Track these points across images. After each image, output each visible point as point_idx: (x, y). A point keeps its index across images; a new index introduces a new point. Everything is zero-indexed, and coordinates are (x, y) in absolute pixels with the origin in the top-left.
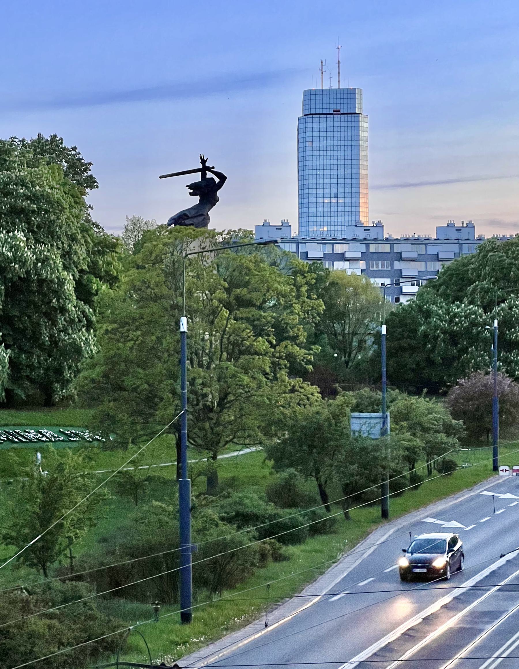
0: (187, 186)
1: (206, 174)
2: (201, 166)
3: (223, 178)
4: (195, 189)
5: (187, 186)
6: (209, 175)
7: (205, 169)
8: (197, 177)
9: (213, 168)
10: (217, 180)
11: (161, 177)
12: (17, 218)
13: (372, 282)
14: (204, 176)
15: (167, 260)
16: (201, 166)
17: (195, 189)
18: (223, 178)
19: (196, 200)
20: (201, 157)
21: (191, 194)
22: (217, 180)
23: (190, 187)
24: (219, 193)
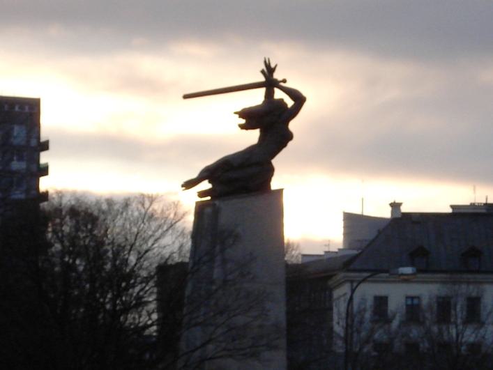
0: (236, 113)
1: (273, 92)
2: (262, 79)
3: (299, 99)
4: (251, 118)
5: (236, 113)
6: (278, 94)
7: (270, 83)
8: (256, 98)
9: (284, 81)
10: (290, 103)
11: (186, 97)
12: (104, 269)
13: (15, 134)
14: (269, 95)
15: (143, 236)
16: (262, 79)
17: (251, 118)
18: (299, 99)
19: (253, 137)
20: (265, 62)
21: (242, 127)
22: (290, 103)
23: (242, 114)
24: (293, 125)
